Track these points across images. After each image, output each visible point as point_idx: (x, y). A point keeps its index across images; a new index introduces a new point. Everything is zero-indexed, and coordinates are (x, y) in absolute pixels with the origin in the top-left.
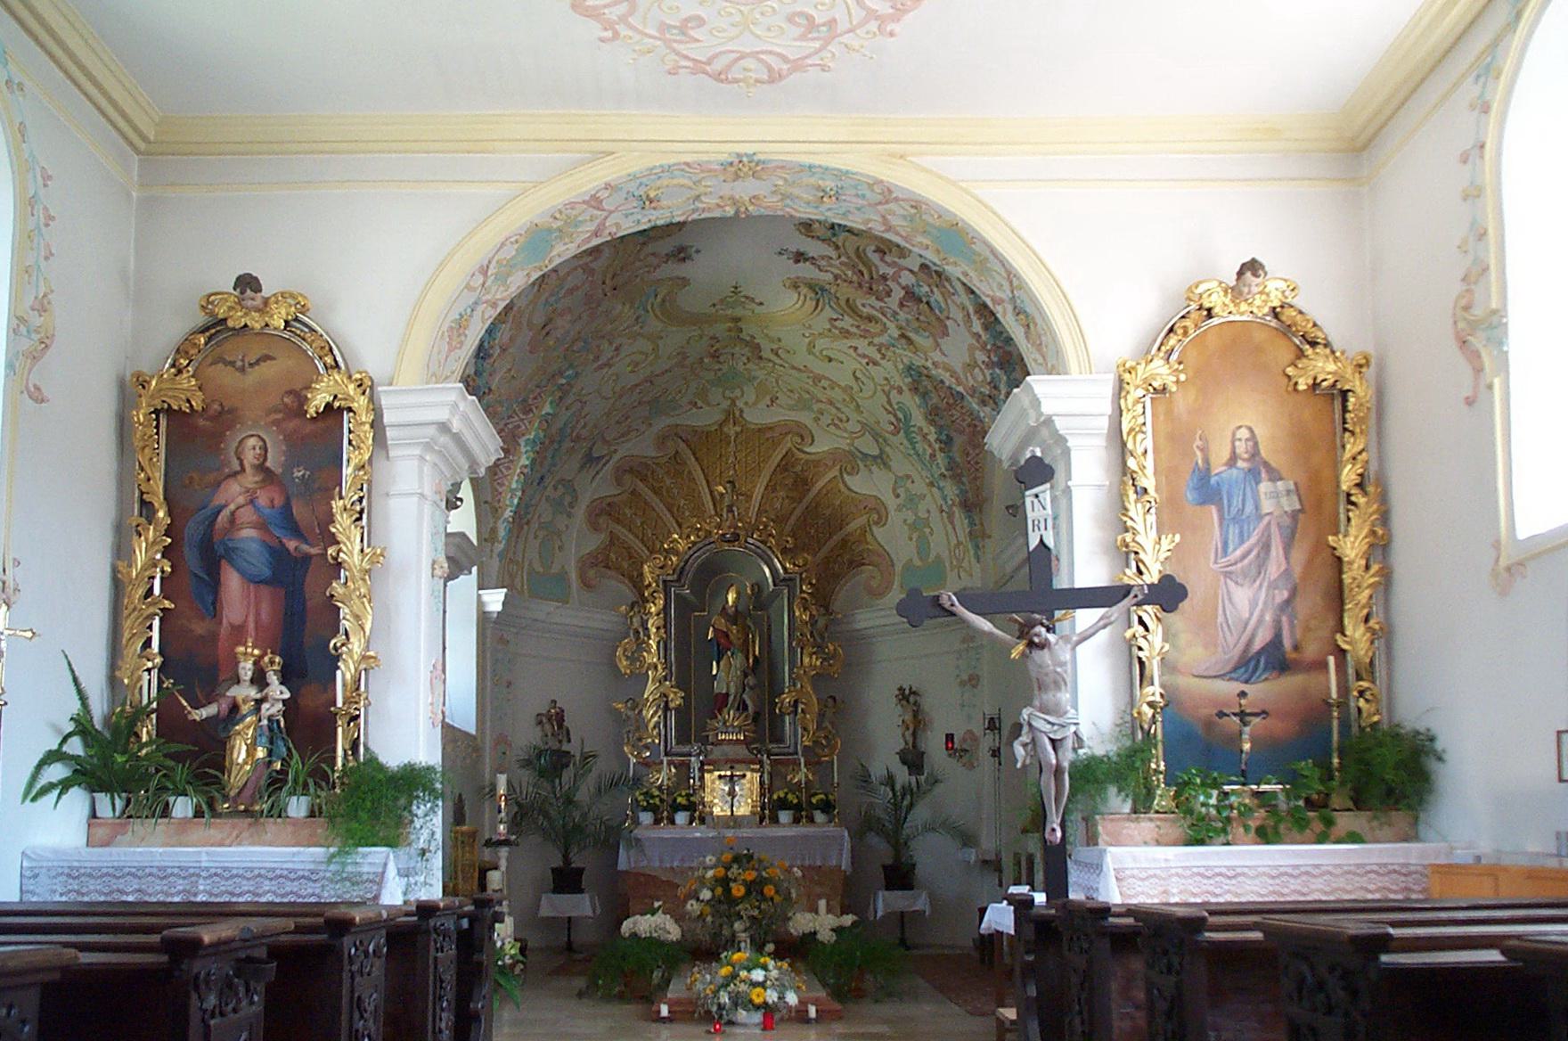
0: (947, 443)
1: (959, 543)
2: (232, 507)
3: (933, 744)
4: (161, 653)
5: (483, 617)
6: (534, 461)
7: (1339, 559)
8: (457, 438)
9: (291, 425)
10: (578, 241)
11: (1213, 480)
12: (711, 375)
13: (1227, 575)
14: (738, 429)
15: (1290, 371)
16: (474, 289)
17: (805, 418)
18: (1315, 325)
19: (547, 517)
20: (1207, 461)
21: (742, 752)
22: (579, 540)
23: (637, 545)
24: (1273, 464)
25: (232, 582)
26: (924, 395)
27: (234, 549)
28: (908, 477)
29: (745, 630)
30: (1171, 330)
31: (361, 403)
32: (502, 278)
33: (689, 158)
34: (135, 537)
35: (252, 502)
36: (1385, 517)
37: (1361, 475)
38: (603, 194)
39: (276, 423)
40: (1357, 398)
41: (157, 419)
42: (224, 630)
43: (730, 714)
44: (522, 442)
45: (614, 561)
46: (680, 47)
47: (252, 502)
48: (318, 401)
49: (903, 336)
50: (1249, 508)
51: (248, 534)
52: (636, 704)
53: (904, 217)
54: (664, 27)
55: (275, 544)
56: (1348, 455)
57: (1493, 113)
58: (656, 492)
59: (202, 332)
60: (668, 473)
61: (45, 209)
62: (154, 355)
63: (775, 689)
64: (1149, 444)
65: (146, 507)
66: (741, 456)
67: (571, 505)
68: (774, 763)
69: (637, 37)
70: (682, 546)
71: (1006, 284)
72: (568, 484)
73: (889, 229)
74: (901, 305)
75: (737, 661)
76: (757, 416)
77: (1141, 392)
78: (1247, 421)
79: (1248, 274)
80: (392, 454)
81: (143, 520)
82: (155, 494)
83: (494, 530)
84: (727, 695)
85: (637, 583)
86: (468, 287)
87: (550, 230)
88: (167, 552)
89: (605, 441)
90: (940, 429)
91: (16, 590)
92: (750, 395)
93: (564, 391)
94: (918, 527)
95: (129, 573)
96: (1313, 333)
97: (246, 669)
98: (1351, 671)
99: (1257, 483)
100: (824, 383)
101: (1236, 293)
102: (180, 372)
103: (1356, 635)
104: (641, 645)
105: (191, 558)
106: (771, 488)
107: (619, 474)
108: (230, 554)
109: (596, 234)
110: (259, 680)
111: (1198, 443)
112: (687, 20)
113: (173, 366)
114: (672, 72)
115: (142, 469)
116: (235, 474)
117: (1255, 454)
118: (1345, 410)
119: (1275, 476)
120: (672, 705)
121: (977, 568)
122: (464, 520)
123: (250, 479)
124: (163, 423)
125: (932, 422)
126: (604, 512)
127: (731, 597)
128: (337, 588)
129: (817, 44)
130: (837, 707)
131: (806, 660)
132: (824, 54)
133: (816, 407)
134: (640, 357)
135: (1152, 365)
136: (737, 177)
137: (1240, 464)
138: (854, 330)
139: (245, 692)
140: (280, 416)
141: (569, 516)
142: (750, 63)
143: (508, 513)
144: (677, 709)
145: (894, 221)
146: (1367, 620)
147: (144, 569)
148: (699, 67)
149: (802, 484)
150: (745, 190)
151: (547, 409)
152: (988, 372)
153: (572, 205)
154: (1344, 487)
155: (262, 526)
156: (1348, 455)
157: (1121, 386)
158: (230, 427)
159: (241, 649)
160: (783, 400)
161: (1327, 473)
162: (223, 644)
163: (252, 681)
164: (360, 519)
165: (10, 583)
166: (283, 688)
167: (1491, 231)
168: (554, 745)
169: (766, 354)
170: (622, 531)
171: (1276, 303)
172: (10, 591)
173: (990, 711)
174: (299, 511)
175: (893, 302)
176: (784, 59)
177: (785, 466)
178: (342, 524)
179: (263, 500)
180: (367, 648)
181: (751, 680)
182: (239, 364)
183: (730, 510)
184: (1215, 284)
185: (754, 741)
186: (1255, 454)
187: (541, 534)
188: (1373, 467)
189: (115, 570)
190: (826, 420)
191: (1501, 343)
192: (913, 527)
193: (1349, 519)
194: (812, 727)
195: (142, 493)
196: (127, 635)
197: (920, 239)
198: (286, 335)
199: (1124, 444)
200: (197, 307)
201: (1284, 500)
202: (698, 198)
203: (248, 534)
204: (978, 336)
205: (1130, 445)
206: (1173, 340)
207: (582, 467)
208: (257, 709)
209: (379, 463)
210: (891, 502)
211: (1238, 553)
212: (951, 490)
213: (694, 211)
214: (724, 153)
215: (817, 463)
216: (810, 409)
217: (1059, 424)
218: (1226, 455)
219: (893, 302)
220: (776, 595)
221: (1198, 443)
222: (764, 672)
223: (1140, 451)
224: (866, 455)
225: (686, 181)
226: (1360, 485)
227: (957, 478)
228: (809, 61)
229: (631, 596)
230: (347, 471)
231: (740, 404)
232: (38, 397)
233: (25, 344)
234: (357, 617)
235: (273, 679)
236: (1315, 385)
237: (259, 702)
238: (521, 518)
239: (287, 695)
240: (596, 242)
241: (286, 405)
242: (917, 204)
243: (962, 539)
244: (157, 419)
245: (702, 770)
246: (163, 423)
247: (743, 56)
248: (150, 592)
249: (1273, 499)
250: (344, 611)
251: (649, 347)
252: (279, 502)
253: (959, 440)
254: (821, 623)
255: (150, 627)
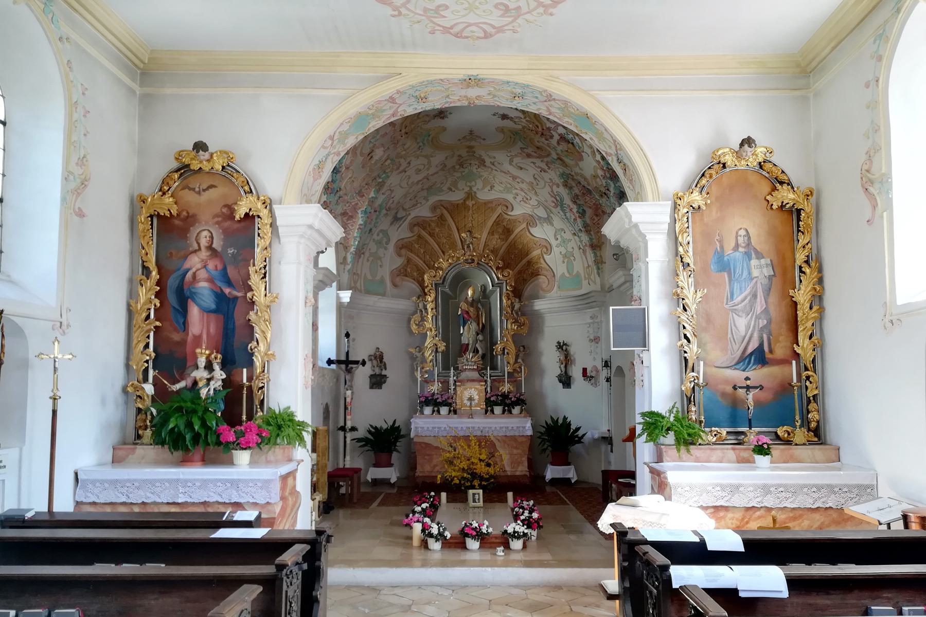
0: (582, 214)
1: (589, 266)
2: (194, 270)
3: (576, 372)
4: (154, 351)
5: (340, 306)
6: (365, 223)
7: (796, 304)
8: (319, 231)
9: (227, 224)
10: (384, 119)
11: (726, 259)
12: (459, 175)
13: (734, 311)
14: (474, 202)
15: (769, 198)
16: (326, 148)
17: (509, 197)
18: (783, 172)
19: (373, 251)
20: (722, 247)
21: (475, 375)
22: (391, 261)
23: (420, 263)
24: (758, 248)
25: (194, 312)
26: (571, 188)
27: (195, 293)
28: (562, 230)
29: (478, 309)
30: (703, 175)
31: (264, 213)
32: (342, 140)
33: (442, 77)
34: (139, 286)
35: (205, 267)
36: (820, 281)
37: (808, 256)
38: (396, 96)
39: (218, 223)
40: (807, 213)
41: (152, 221)
42: (190, 338)
43: (470, 355)
44: (359, 212)
45: (410, 272)
46: (436, 20)
47: (205, 267)
48: (241, 212)
49: (559, 159)
50: (745, 273)
51: (203, 286)
52: (421, 348)
53: (559, 109)
54: (426, 10)
55: (219, 291)
56: (800, 245)
57: (884, 61)
58: (431, 235)
59: (177, 171)
60: (437, 226)
61: (84, 107)
62: (150, 186)
63: (493, 343)
64: (690, 239)
65: (146, 271)
66: (475, 216)
67: (387, 243)
68: (493, 381)
69: (412, 15)
70: (445, 265)
71: (613, 148)
72: (384, 232)
73: (550, 114)
74: (558, 143)
75: (473, 326)
76: (484, 195)
77: (685, 210)
78: (746, 224)
79: (746, 146)
80: (282, 240)
81: (144, 277)
82: (150, 261)
83: (345, 258)
84: (468, 345)
85: (421, 284)
86: (323, 147)
87: (368, 115)
88: (157, 295)
89: (404, 209)
90: (579, 206)
91: (68, 326)
92: (480, 184)
93: (381, 186)
94: (568, 257)
95: (136, 307)
96: (782, 177)
97: (202, 362)
98: (802, 365)
99: (750, 259)
100: (518, 180)
101: (738, 155)
102: (164, 194)
103: (805, 346)
104: (423, 319)
105: (172, 298)
106: (491, 233)
107: (412, 226)
108: (193, 296)
109: (393, 115)
110: (209, 367)
111: (717, 237)
112: (439, 6)
113: (160, 190)
114: (432, 32)
115: (143, 248)
116: (195, 251)
117: (749, 244)
118: (799, 220)
119: (759, 256)
120: (440, 350)
121: (598, 280)
122: (328, 260)
123: (204, 254)
124: (155, 220)
125: (575, 202)
126: (403, 247)
127: (470, 292)
128: (252, 316)
129: (510, 19)
130: (525, 349)
131: (509, 326)
132: (515, 24)
133: (514, 191)
134: (421, 167)
135: (693, 195)
136: (468, 87)
137: (741, 249)
138: (534, 154)
139: (201, 374)
140: (220, 219)
141: (386, 249)
142: (473, 28)
143: (352, 249)
144: (443, 352)
145: (553, 110)
146: (811, 337)
147: (144, 304)
148: (446, 30)
149: (508, 231)
150: (473, 93)
151: (372, 195)
152: (604, 181)
153: (379, 102)
154: (798, 263)
155: (211, 280)
156: (800, 245)
157: (675, 207)
158: (193, 225)
159: (198, 351)
160: (497, 187)
161: (788, 255)
162: (188, 349)
163: (205, 368)
164: (265, 277)
165: (65, 323)
166: (222, 373)
167: (882, 128)
168: (377, 371)
169: (488, 163)
170: (412, 256)
171: (761, 160)
172: (64, 327)
173: (605, 358)
174: (231, 272)
175: (554, 142)
176: (494, 27)
177: (497, 223)
178: (255, 280)
179: (211, 265)
180: (269, 350)
181: (480, 337)
182: (197, 189)
183: (468, 247)
184: (728, 150)
185: (482, 369)
186: (749, 244)
187: (371, 259)
188: (814, 252)
189: (129, 306)
190: (519, 198)
191: (888, 193)
192: (565, 256)
193: (801, 281)
194: (512, 362)
195: (143, 262)
196: (135, 342)
197: (567, 119)
198: (223, 173)
199: (676, 238)
200: (173, 159)
201: (765, 270)
202: (448, 96)
203: (203, 286)
204: (598, 162)
205: (680, 239)
206: (704, 181)
207: (391, 224)
208: (208, 384)
209: (275, 245)
210: (554, 243)
211: (740, 298)
212: (585, 238)
213: (447, 102)
214: (461, 74)
215: (515, 221)
216: (511, 192)
217: (642, 228)
218: (733, 244)
219: (554, 142)
220: (493, 292)
221: (717, 237)
222: (486, 330)
223: (685, 242)
224: (540, 218)
225: (439, 88)
226: (807, 262)
227: (588, 232)
228: (506, 28)
229: (415, 287)
230: (257, 250)
231: (474, 189)
232: (81, 214)
233: (73, 185)
234: (263, 332)
235: (217, 367)
236: (782, 206)
237: (209, 380)
238: (359, 253)
239: (224, 376)
240: (392, 119)
241: (223, 213)
242: (566, 103)
243: (590, 263)
244: (152, 221)
245: (455, 384)
246: (155, 220)
247: (470, 25)
248: (148, 317)
249: (760, 270)
250: (257, 329)
251: (425, 161)
252: (220, 267)
253: (589, 212)
254: (517, 306)
255: (148, 337)
